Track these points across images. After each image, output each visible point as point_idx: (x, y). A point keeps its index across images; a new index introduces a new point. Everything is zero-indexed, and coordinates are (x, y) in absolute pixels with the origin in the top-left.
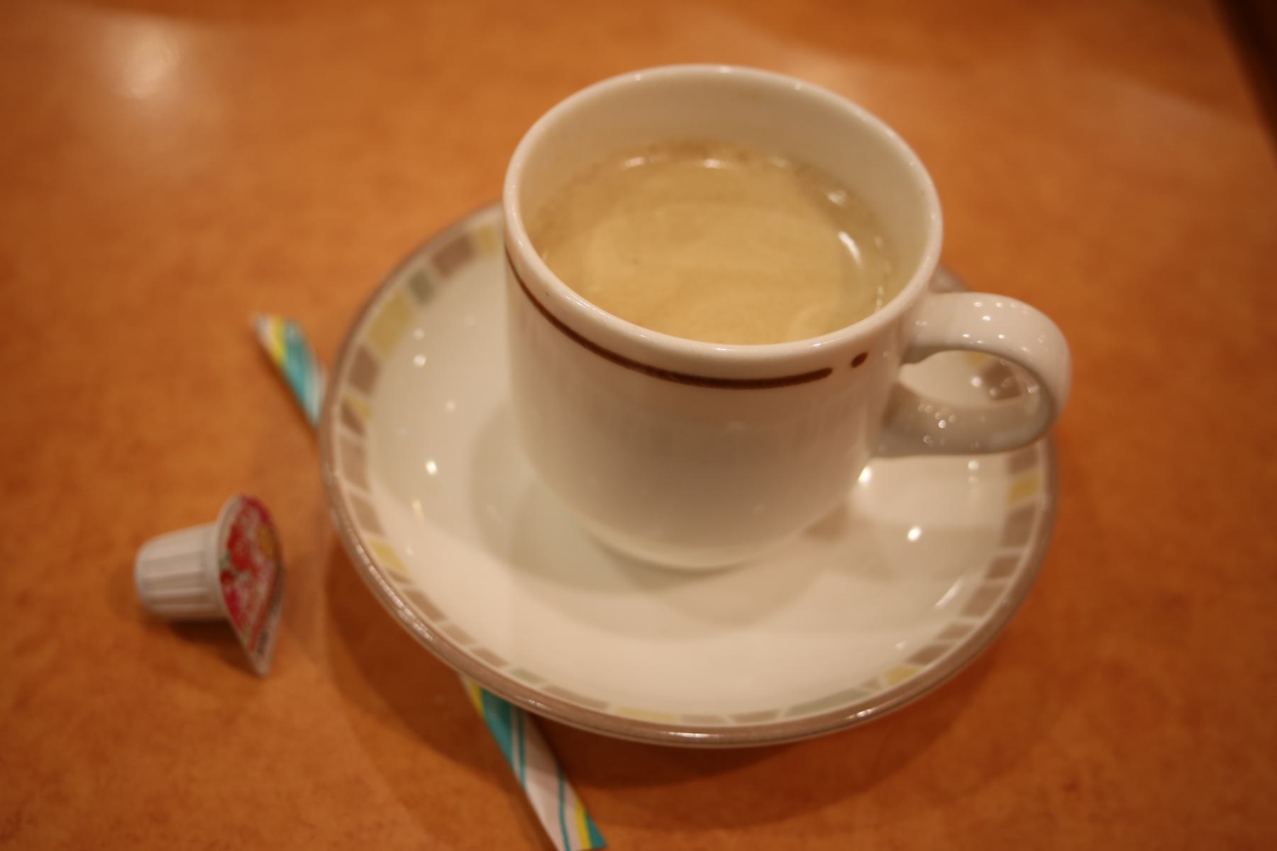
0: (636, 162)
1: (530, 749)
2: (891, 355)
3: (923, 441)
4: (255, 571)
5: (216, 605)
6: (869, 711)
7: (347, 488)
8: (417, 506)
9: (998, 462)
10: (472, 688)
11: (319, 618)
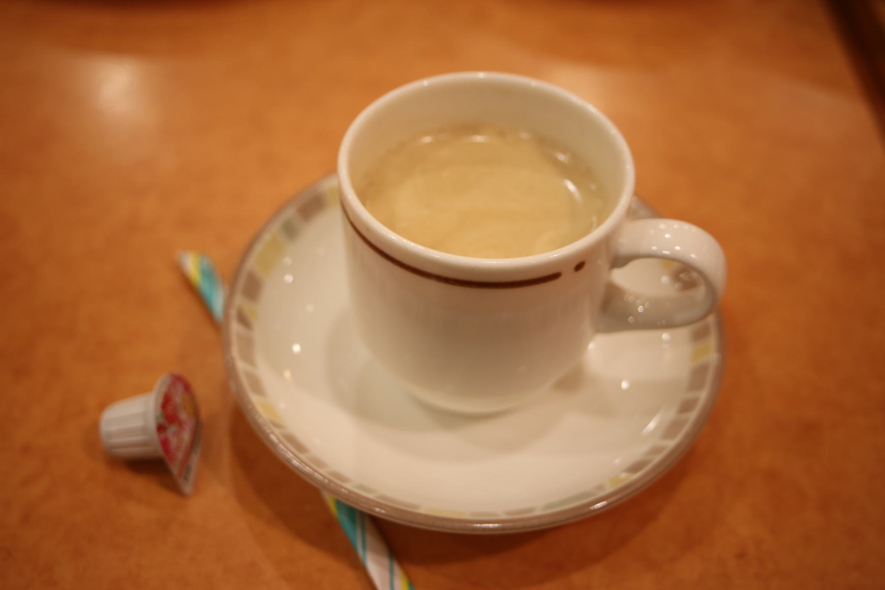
0: (427, 140)
1: (371, 540)
2: (603, 262)
3: (628, 321)
4: (180, 424)
5: (155, 448)
6: (496, 525)
7: (241, 365)
8: (287, 374)
9: (684, 333)
10: (329, 499)
11: (226, 456)
